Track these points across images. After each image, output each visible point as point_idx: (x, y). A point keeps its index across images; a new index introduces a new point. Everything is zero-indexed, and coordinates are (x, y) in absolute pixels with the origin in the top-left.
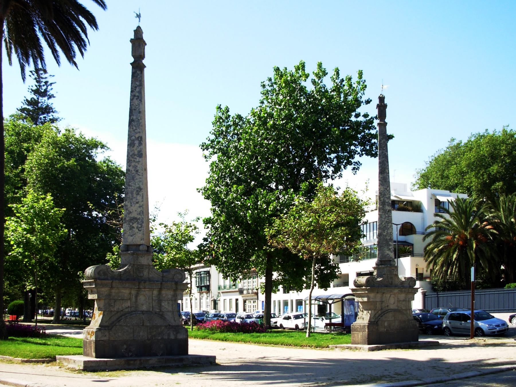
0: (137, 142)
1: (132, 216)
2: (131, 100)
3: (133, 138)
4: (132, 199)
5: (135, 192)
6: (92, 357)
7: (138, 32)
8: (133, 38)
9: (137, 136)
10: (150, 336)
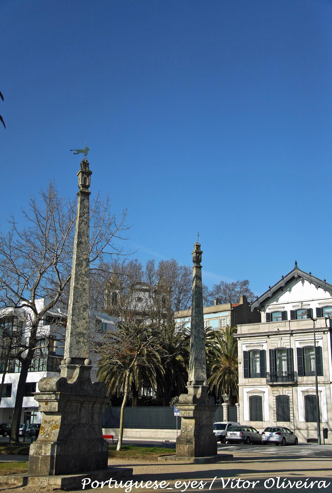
0: (84, 263)
1: (78, 330)
3: (81, 258)
4: (79, 315)
5: (82, 309)
7: (296, 262)
9: (85, 257)
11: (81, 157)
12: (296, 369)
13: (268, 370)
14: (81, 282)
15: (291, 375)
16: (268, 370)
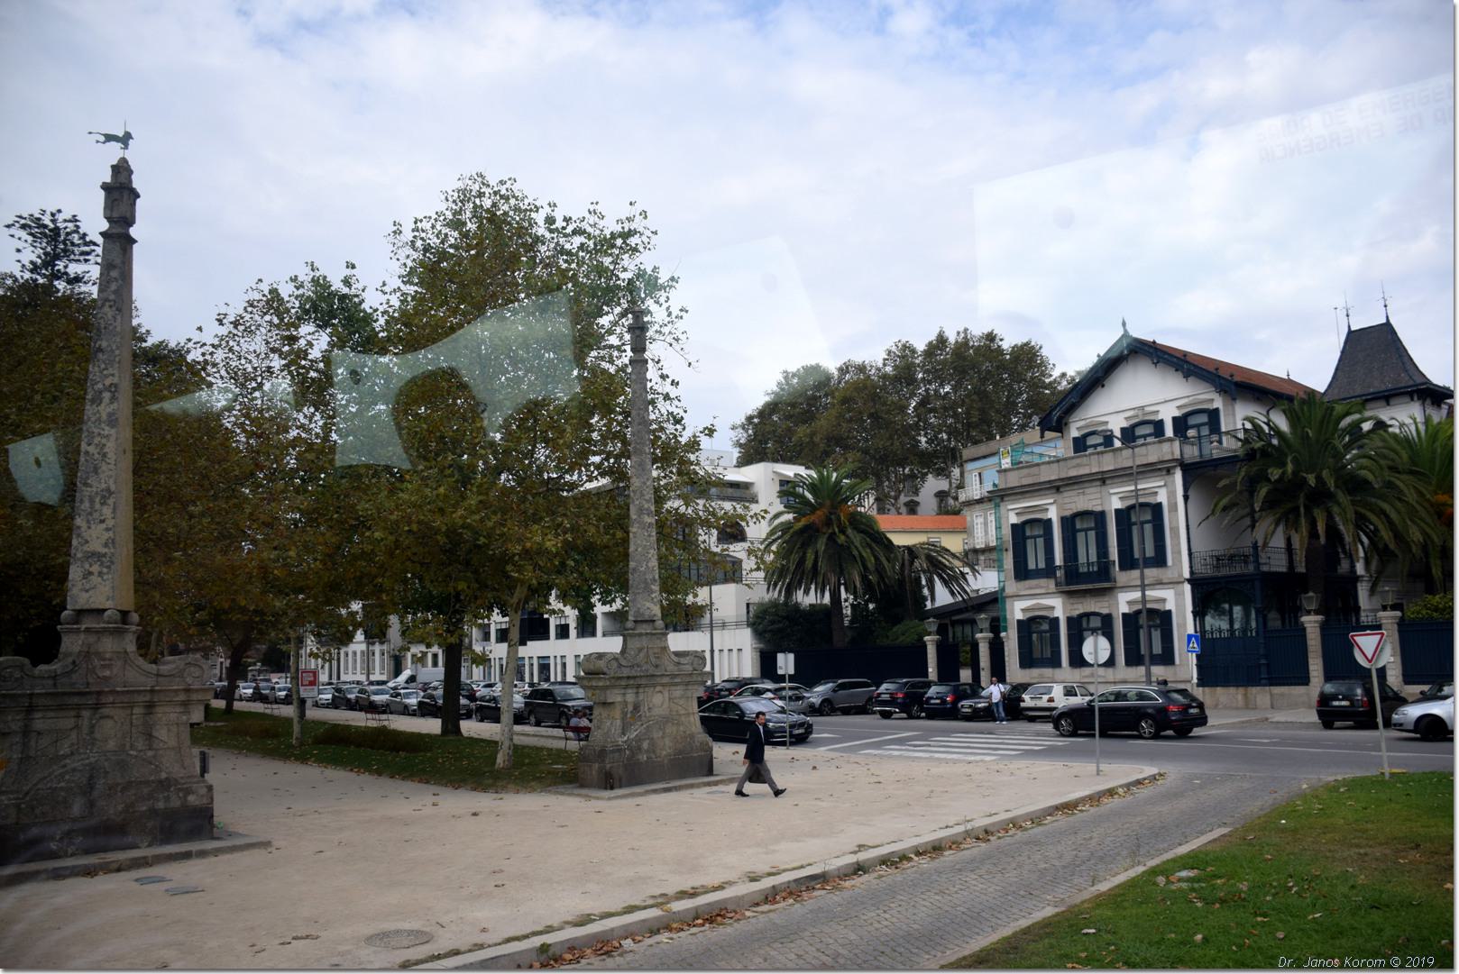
0: (107, 395)
7: (122, 170)
8: (108, 180)
11: (114, 152)
12: (1114, 554)
13: (1059, 559)
14: (97, 440)
15: (1104, 572)
16: (1059, 559)
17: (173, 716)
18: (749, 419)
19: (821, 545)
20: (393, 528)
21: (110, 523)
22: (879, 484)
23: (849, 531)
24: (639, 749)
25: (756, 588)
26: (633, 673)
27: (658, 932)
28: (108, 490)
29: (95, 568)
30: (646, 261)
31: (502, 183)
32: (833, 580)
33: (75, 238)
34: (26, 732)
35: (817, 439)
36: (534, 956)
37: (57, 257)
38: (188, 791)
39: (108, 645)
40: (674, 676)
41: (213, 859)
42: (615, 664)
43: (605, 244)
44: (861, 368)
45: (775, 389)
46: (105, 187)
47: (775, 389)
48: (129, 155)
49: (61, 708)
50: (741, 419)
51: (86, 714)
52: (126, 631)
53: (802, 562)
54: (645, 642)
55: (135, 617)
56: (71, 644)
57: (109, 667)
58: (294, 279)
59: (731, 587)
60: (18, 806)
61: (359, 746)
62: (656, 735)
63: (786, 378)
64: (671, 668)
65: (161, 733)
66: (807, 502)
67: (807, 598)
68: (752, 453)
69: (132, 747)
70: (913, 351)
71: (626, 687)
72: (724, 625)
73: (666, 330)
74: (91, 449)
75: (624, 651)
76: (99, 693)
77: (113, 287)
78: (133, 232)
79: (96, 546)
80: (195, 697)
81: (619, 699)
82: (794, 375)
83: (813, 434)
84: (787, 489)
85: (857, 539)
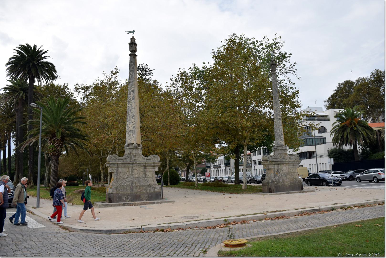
0: (132, 92)
2: (129, 72)
6: (107, 202)
7: (133, 39)
8: (130, 42)
10: (139, 191)
11: (131, 35)
17: (151, 170)
18: (329, 98)
19: (348, 130)
20: (207, 122)
21: (134, 123)
22: (373, 114)
23: (357, 126)
24: (279, 182)
25: (330, 145)
26: (277, 160)
27: (262, 220)
28: (133, 115)
29: (131, 134)
30: (282, 50)
31: (241, 35)
32: (353, 141)
33: (147, 70)
34: (117, 172)
35: (350, 102)
36: (223, 222)
37: (143, 75)
38: (155, 188)
39: (135, 152)
40: (289, 161)
41: (160, 204)
42: (271, 158)
43: (269, 46)
44: (363, 80)
45: (336, 89)
46: (129, 44)
47: (336, 89)
48: (134, 36)
49: (125, 167)
50: (326, 99)
51: (130, 168)
52: (139, 149)
53: (342, 136)
54: (280, 152)
55: (141, 145)
56: (127, 152)
57: (135, 157)
58: (190, 68)
59: (323, 145)
60: (116, 189)
61: (212, 186)
62: (285, 178)
63: (339, 85)
64: (288, 159)
65: (148, 173)
66: (344, 119)
67: (347, 148)
68: (329, 108)
69: (141, 177)
70: (381, 72)
71: (274, 164)
72: (321, 156)
73: (290, 70)
74: (129, 106)
75: (274, 155)
76: (133, 163)
77: (132, 67)
78: (136, 53)
79: (131, 128)
80: (156, 165)
81: (273, 168)
82: (342, 84)
83: (349, 101)
84: (338, 116)
85: (360, 128)
